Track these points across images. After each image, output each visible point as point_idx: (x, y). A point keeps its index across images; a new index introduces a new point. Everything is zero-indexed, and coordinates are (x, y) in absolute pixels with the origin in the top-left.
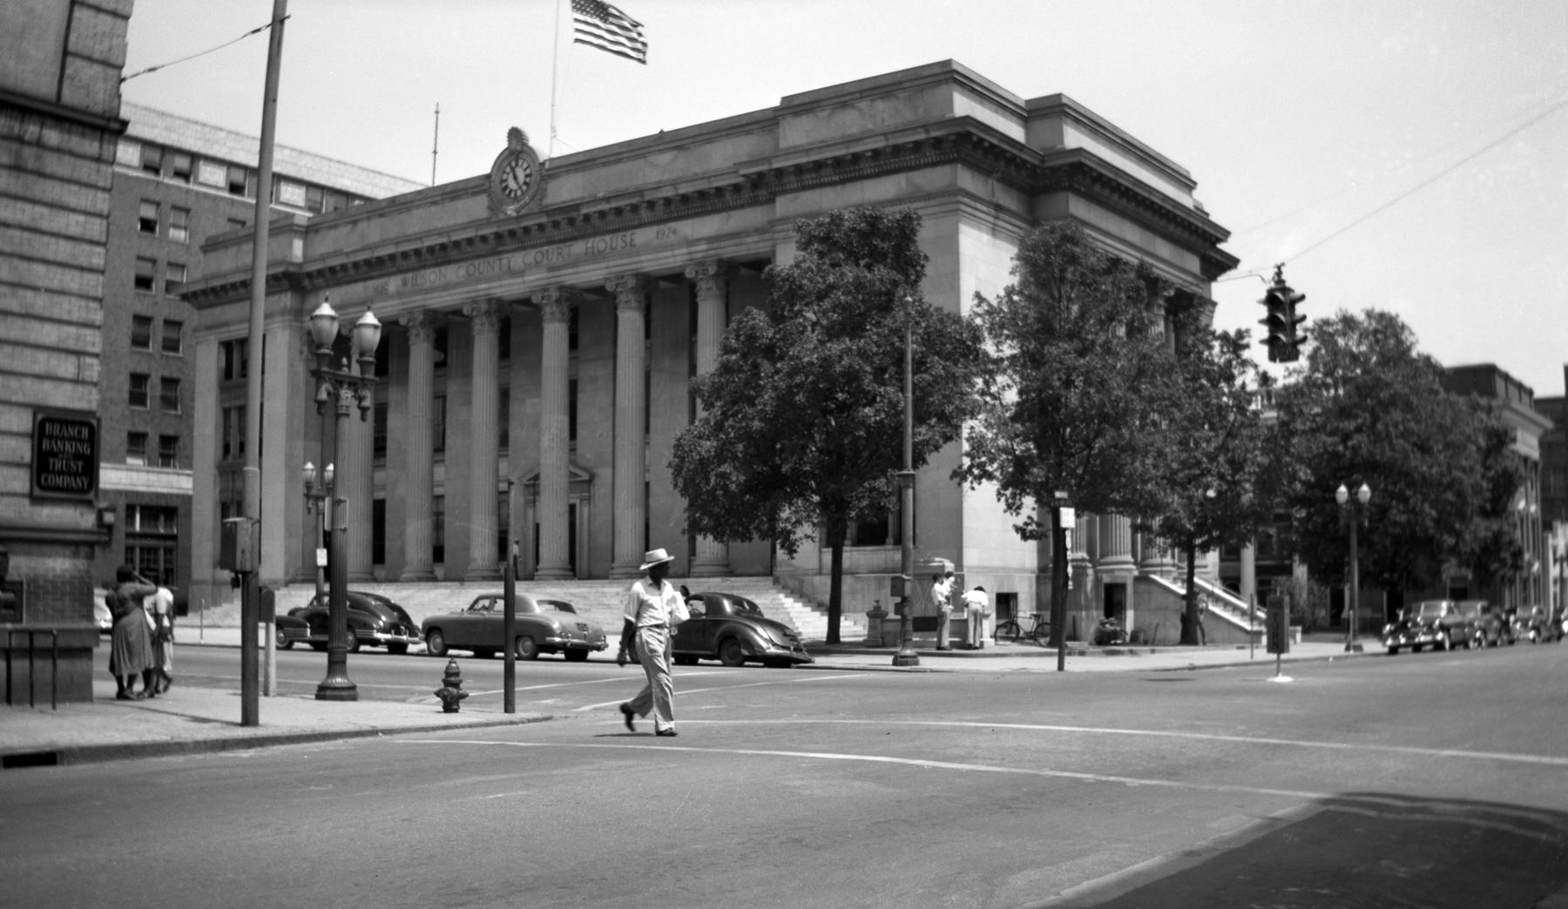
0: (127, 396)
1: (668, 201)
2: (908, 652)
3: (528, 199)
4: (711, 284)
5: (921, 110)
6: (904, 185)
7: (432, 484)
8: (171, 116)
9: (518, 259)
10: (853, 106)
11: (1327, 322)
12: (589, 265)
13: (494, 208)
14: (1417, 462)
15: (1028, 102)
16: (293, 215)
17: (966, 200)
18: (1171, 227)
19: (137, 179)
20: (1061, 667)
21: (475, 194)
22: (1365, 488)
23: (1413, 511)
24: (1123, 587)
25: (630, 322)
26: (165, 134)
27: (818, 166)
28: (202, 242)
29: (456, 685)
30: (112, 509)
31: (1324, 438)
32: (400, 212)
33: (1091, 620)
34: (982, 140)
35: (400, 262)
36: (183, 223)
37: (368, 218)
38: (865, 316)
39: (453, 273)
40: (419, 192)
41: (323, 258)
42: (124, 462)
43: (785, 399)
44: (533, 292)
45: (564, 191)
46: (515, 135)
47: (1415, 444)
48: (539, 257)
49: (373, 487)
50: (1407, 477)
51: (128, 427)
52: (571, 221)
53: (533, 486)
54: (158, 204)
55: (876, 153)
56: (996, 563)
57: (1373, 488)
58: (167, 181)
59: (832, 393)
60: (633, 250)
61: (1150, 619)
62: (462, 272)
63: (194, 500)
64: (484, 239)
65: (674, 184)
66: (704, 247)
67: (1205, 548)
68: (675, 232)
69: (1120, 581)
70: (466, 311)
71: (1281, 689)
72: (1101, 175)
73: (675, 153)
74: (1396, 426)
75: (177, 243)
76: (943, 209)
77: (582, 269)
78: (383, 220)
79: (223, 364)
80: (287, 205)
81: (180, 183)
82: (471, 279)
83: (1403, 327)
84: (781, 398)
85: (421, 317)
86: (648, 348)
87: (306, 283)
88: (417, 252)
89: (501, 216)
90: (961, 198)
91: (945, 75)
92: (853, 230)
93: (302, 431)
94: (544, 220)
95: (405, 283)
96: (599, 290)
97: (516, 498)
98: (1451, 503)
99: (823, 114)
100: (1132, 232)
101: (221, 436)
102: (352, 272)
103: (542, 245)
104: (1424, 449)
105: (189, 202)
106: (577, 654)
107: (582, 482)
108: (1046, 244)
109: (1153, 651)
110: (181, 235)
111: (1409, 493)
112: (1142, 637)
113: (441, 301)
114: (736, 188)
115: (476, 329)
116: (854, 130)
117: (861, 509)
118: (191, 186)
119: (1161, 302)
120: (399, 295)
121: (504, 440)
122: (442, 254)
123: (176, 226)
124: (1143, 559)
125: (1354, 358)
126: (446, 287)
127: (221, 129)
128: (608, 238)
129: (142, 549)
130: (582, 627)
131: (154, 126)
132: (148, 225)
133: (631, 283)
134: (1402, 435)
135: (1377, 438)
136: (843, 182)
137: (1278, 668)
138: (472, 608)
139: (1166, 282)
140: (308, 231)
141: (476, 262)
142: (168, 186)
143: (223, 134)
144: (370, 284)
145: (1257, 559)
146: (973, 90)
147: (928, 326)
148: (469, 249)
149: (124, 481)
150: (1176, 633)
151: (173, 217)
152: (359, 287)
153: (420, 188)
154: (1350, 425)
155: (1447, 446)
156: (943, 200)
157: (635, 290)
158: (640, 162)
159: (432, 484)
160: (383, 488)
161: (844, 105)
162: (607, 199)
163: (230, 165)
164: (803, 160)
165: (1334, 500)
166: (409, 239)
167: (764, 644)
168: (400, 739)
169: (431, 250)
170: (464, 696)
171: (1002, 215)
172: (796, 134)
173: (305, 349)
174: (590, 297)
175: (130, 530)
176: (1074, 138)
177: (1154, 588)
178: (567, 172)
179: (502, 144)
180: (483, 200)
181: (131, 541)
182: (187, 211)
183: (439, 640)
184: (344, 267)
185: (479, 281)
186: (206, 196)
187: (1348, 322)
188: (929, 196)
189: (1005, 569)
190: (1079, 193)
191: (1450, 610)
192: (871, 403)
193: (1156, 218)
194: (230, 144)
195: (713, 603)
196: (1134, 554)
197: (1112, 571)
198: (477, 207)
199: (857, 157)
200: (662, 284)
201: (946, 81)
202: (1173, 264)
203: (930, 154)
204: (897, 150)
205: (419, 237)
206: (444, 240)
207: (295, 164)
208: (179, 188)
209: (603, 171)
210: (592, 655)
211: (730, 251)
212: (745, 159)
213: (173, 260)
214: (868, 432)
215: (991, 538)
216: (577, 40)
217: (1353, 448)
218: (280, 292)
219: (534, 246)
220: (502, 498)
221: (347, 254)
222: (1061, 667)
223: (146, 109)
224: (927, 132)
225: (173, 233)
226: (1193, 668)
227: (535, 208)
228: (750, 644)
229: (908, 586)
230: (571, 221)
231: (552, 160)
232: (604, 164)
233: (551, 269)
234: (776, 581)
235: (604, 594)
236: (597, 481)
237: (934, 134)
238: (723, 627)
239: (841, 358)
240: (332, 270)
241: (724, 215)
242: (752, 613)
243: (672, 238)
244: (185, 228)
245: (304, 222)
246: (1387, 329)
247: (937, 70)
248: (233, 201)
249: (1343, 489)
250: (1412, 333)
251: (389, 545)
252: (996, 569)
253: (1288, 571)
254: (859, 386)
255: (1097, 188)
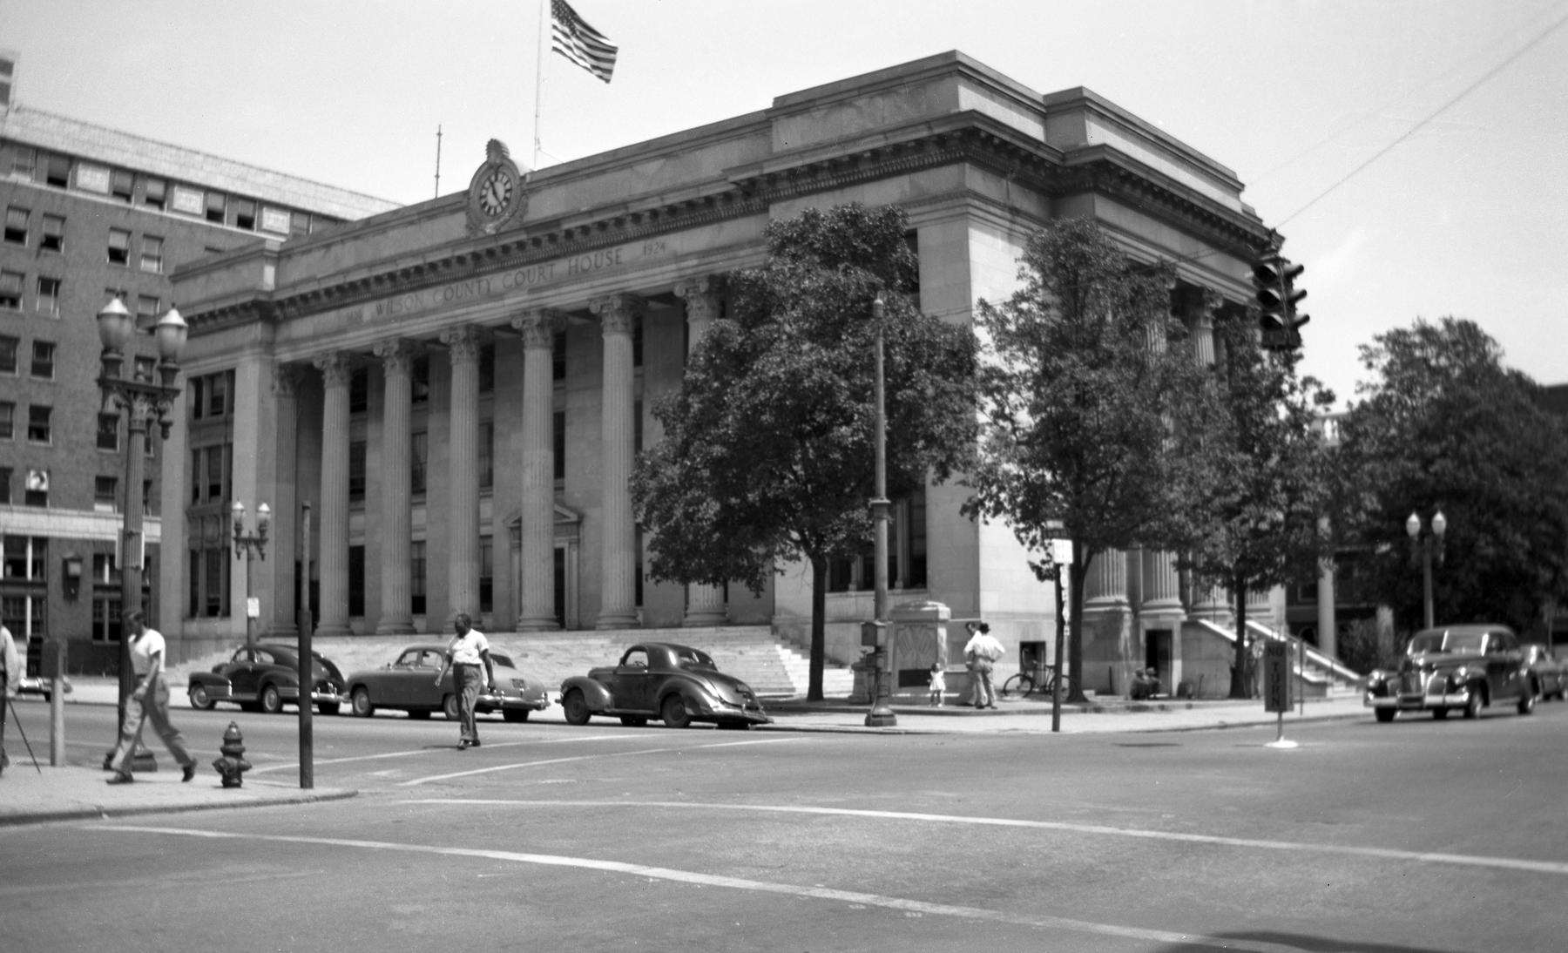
0: (94, 438)
1: (654, 213)
2: (883, 710)
3: (507, 219)
4: (703, 302)
5: (924, 106)
6: (907, 188)
7: (410, 529)
8: (144, 139)
9: (497, 281)
10: (850, 105)
11: (1401, 333)
12: (572, 286)
13: (472, 226)
14: (1508, 489)
15: (1046, 97)
16: (263, 241)
17: (977, 203)
18: (1216, 232)
19: (107, 206)
20: (1056, 727)
21: (453, 212)
22: (1439, 518)
23: (1504, 544)
24: (1168, 634)
25: (616, 346)
26: (238, 183)
27: (813, 170)
28: (171, 271)
29: (238, 755)
30: (78, 560)
31: (1402, 462)
32: (375, 233)
33: (1131, 669)
34: (991, 137)
35: (374, 287)
36: (156, 252)
37: (342, 241)
38: (842, 323)
39: (430, 297)
40: (395, 212)
41: (294, 285)
42: (92, 509)
43: (749, 421)
44: (513, 316)
45: (545, 206)
46: (495, 147)
47: (1504, 468)
48: (520, 278)
49: (348, 533)
50: (1497, 506)
51: (97, 471)
52: (553, 238)
53: (516, 529)
54: (129, 233)
55: (876, 154)
56: (1020, 608)
57: (1449, 519)
58: (138, 208)
59: (805, 410)
60: (618, 268)
61: (1197, 669)
62: (439, 297)
63: (163, 548)
64: (461, 260)
65: (661, 194)
66: (695, 262)
67: (1262, 586)
68: (663, 247)
69: (1164, 627)
70: (443, 339)
71: (1278, 754)
72: (1130, 175)
73: (662, 161)
74: (1481, 448)
75: (150, 274)
76: (951, 212)
77: (564, 290)
78: (359, 242)
79: (193, 402)
80: (85, 191)
81: (155, 211)
82: (448, 304)
83: (1486, 338)
84: (745, 417)
85: (396, 347)
86: (636, 376)
87: (278, 312)
88: (392, 276)
89: (480, 235)
90: (969, 200)
91: (950, 67)
92: (832, 230)
93: (274, 473)
94: (523, 237)
95: (380, 310)
96: (584, 313)
97: (501, 544)
98: (1546, 534)
99: (818, 114)
100: (1171, 239)
101: (190, 480)
102: (324, 299)
103: (523, 264)
104: (1513, 472)
105: (163, 230)
106: (516, 714)
107: (570, 523)
108: (1054, 244)
109: (1189, 707)
110: (153, 266)
111: (1498, 523)
112: (1190, 690)
113: (417, 328)
114: (727, 197)
115: (454, 358)
116: (853, 130)
117: (837, 543)
118: (165, 213)
119: (1208, 314)
120: (374, 323)
121: (487, 481)
122: (417, 277)
123: (148, 257)
124: (1195, 602)
125: (1435, 371)
126: (421, 314)
127: (198, 153)
128: (592, 255)
129: (111, 603)
130: (518, 683)
131: (123, 151)
132: (117, 255)
133: (617, 303)
134: (1490, 458)
135: (1462, 462)
136: (841, 186)
137: (1280, 729)
138: (399, 662)
139: (1212, 292)
140: (281, 257)
141: (454, 285)
142: (140, 213)
143: (200, 158)
144: (344, 312)
145: (1336, 602)
146: (981, 84)
147: (913, 336)
148: (446, 271)
149: (46, 526)
150: (1226, 685)
151: (145, 247)
152: (332, 315)
153: (394, 208)
154: (1435, 449)
155: (1541, 469)
156: (950, 203)
157: (621, 311)
158: (626, 173)
159: (410, 529)
160: (362, 533)
161: (841, 103)
162: (590, 213)
163: (208, 190)
164: (797, 163)
165: (1404, 532)
166: (384, 262)
167: (712, 703)
168: (88, 825)
169: (406, 273)
170: (246, 768)
171: (1019, 220)
172: (791, 137)
173: (277, 384)
174: (578, 321)
175: (98, 582)
176: (1098, 134)
177: (1204, 635)
178: (549, 185)
179: (481, 157)
180: (461, 218)
181: (99, 594)
182: (161, 240)
183: (364, 699)
184: (316, 294)
185: (457, 306)
186: (181, 223)
187: (1426, 332)
188: (935, 199)
189: (1031, 615)
190: (1106, 194)
191: (1541, 656)
192: (848, 421)
193: (1198, 222)
194: (207, 168)
195: (657, 656)
196: (1183, 596)
197: (1157, 616)
198: (455, 226)
199: (855, 159)
200: (653, 305)
201: (950, 74)
202: (1231, 280)
203: (935, 153)
204: (898, 149)
205: (392, 260)
206: (419, 262)
207: (278, 189)
208: (151, 215)
209: (588, 183)
210: (533, 715)
211: (720, 265)
212: (736, 163)
213: (145, 291)
214: (845, 455)
215: (1012, 577)
216: (555, 49)
217: (1435, 474)
218: (251, 322)
219: (514, 267)
220: (484, 543)
221: (319, 280)
222: (1056, 727)
223: (116, 132)
224: (930, 128)
225: (146, 265)
226: (1224, 726)
227: (514, 224)
228: (696, 702)
229: (881, 634)
230: (553, 238)
231: (533, 173)
232: (588, 176)
233: (531, 291)
234: (775, 631)
235: (588, 647)
236: (586, 522)
237: (937, 131)
238: (668, 682)
239: (810, 371)
240: (304, 297)
241: (715, 226)
242: (705, 667)
243: (661, 254)
244: (159, 259)
245: (277, 248)
246: (1467, 337)
247: (940, 63)
248: (211, 229)
249: (1414, 519)
250: (1495, 344)
251: (368, 596)
252: (1021, 615)
253: (1371, 613)
254: (833, 403)
255: (1127, 189)
